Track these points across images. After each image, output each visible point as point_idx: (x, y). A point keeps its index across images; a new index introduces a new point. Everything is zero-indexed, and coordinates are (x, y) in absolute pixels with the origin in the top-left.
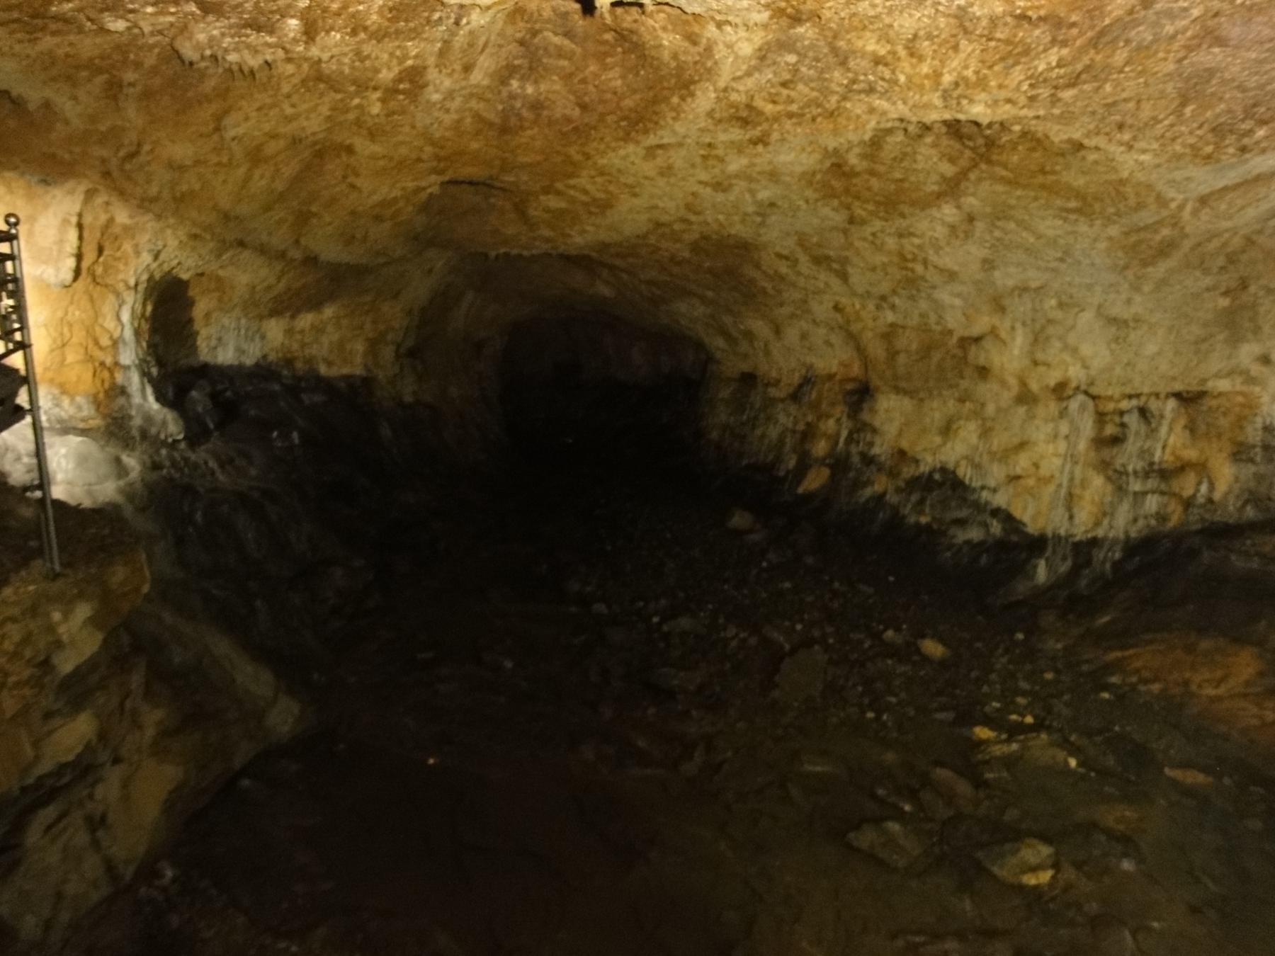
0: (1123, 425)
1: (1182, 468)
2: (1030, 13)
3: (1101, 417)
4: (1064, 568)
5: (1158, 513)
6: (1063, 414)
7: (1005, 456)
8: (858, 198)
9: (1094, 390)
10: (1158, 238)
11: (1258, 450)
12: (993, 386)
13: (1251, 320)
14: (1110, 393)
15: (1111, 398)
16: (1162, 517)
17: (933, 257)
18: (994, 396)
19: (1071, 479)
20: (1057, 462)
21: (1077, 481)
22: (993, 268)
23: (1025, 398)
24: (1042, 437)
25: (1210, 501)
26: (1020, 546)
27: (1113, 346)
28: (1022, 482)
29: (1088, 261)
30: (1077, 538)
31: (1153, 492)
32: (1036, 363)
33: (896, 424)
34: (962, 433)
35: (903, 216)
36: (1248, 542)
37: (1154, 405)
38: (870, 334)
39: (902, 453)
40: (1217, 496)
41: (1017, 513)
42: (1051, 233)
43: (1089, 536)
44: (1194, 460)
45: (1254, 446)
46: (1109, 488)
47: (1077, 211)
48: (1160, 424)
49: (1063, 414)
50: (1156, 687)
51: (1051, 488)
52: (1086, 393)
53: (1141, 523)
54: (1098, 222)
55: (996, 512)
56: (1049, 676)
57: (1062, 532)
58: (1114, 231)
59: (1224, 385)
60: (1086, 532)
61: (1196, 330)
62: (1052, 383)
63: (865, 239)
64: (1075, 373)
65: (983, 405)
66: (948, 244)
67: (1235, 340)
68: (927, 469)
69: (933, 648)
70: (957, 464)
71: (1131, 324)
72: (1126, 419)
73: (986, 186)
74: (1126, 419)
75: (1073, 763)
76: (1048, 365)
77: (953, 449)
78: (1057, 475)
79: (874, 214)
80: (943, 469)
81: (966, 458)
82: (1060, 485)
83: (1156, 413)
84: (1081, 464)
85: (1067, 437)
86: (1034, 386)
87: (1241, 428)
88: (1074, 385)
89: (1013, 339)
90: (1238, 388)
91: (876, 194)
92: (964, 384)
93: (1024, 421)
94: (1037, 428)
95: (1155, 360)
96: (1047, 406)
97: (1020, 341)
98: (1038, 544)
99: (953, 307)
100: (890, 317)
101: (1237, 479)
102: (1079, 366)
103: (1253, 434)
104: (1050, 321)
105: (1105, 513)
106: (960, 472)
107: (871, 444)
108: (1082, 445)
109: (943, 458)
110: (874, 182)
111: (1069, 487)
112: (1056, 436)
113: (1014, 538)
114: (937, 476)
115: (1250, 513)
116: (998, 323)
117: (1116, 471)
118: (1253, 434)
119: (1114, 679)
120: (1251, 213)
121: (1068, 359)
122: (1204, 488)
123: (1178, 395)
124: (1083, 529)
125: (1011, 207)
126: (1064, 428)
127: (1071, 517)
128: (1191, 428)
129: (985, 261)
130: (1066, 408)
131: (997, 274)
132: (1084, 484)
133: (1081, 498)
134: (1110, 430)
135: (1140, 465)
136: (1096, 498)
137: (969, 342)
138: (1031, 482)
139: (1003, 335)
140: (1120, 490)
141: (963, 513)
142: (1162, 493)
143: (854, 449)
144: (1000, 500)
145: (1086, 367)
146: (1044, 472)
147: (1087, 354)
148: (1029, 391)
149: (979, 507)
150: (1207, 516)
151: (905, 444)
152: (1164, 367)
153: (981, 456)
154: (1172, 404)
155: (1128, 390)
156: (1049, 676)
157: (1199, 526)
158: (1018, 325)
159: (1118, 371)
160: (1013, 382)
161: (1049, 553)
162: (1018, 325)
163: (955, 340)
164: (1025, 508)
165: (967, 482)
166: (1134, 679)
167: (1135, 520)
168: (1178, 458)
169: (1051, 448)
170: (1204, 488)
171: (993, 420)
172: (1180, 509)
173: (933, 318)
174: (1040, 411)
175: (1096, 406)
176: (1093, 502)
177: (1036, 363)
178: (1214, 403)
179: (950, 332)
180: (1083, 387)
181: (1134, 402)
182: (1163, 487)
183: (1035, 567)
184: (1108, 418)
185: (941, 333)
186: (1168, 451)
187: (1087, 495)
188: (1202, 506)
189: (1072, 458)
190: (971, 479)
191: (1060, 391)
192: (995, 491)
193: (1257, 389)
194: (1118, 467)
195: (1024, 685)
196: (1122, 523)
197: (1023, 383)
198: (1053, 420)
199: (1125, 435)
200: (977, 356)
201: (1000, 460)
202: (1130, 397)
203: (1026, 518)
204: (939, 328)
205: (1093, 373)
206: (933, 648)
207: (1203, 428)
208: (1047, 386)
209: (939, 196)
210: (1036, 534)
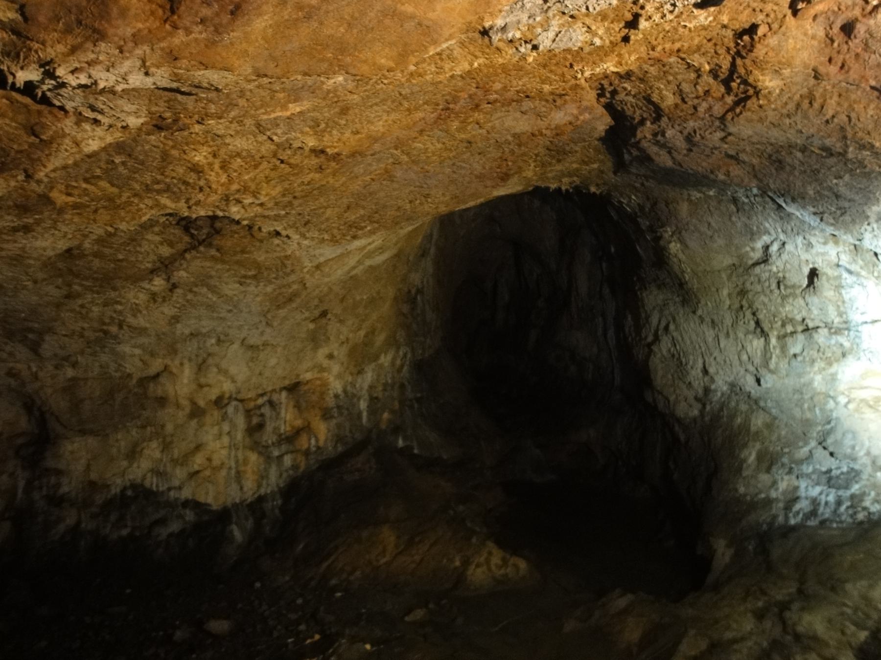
0: (262, 415)
1: (298, 432)
2: (328, 150)
3: (248, 413)
4: (250, 524)
5: (293, 466)
6: (224, 417)
7: (184, 460)
8: (77, 276)
9: (240, 397)
10: (291, 290)
11: (335, 410)
12: (170, 410)
13: (325, 334)
14: (250, 396)
15: (250, 399)
16: (295, 467)
17: (131, 320)
18: (171, 419)
19: (237, 462)
20: (224, 452)
21: (241, 461)
22: (178, 322)
23: (197, 412)
24: (210, 437)
25: (318, 448)
26: (213, 522)
27: (251, 364)
28: (201, 475)
29: (247, 310)
30: (249, 500)
31: (287, 453)
32: (201, 386)
33: (83, 461)
34: (146, 452)
35: (114, 289)
36: (349, 465)
37: (275, 397)
38: (49, 391)
39: (92, 484)
40: (321, 443)
41: (202, 499)
42: (230, 293)
43: (256, 496)
44: (301, 426)
45: (332, 408)
46: (261, 460)
47: (254, 277)
48: (280, 408)
49: (224, 417)
50: (358, 573)
51: (224, 473)
52: (236, 399)
53: (285, 475)
54: (262, 284)
55: (186, 504)
56: (300, 601)
57: (237, 501)
58: (269, 289)
59: (308, 376)
60: (254, 494)
61: (299, 345)
62: (214, 397)
63: (72, 311)
64: (227, 387)
65: (163, 426)
66: (147, 308)
67: (316, 348)
68: (118, 490)
69: (219, 626)
70: (144, 478)
71: (261, 348)
72: (263, 410)
73: (197, 263)
74: (263, 410)
75: (368, 647)
76: (209, 386)
77: (138, 467)
78: (227, 461)
79: (89, 289)
80: (134, 486)
81: (152, 471)
82: (230, 468)
83: (277, 402)
84: (241, 448)
85: (229, 433)
86: (202, 403)
87: (324, 399)
88: (227, 395)
89: (183, 372)
90: (316, 375)
91: (95, 272)
92: (146, 414)
93: (197, 430)
94: (207, 432)
95: (275, 368)
96: (212, 415)
97: (187, 373)
98: (224, 515)
99: (133, 356)
100: (70, 373)
101: (329, 431)
102: (229, 382)
103: (330, 402)
104: (209, 355)
105: (263, 476)
106: (147, 484)
107: (58, 485)
108: (239, 436)
109: (131, 477)
110: (97, 263)
111: (237, 467)
112: (220, 435)
113: (206, 518)
114: (129, 493)
115: (340, 449)
116: (169, 363)
117: (263, 446)
118: (330, 402)
119: (334, 582)
120: (339, 272)
121: (222, 378)
122: (313, 441)
123: (285, 388)
124: (251, 493)
125: (211, 277)
126: (226, 427)
127: (241, 488)
128: (298, 406)
129: (173, 317)
130: (226, 413)
131: (179, 326)
132: (246, 461)
133: (245, 472)
134: (255, 420)
135: (275, 438)
136: (255, 469)
137: (144, 382)
138: (207, 473)
139: (175, 370)
140: (268, 459)
141: (162, 513)
142: (292, 452)
143: (36, 495)
144: (186, 493)
145: (234, 381)
146: (216, 462)
147: (235, 373)
148: (199, 407)
149: (172, 505)
150: (320, 458)
151: (93, 476)
152: (280, 372)
153: (165, 466)
154: (284, 394)
155: (260, 392)
156: (300, 601)
157: (317, 465)
158: (186, 361)
159: (254, 380)
160: (185, 403)
161: (234, 520)
162: (186, 361)
163: (134, 381)
164: (207, 493)
165: (155, 489)
166: (344, 576)
167: (281, 475)
168: (293, 427)
169: (218, 444)
170: (313, 441)
171: (172, 435)
172: (304, 458)
173: (113, 366)
174: (208, 419)
175: (244, 406)
176: (253, 472)
177: (201, 386)
178: (306, 388)
179: (130, 376)
180: (234, 396)
181: (265, 398)
182: (291, 448)
183: (231, 532)
184: (252, 413)
185: (121, 378)
186: (287, 425)
187: (249, 469)
188: (316, 452)
189: (233, 446)
190: (157, 486)
191: (219, 402)
192: (180, 488)
193: (326, 374)
194: (264, 443)
195: (293, 616)
196: (274, 480)
197: (194, 403)
198: (218, 424)
199: (264, 421)
200: (154, 390)
201: (182, 465)
202: (262, 395)
203: (210, 500)
204: (118, 375)
205: (239, 385)
206: (219, 626)
207: (304, 405)
208: (211, 401)
209: (152, 271)
210: (219, 508)
